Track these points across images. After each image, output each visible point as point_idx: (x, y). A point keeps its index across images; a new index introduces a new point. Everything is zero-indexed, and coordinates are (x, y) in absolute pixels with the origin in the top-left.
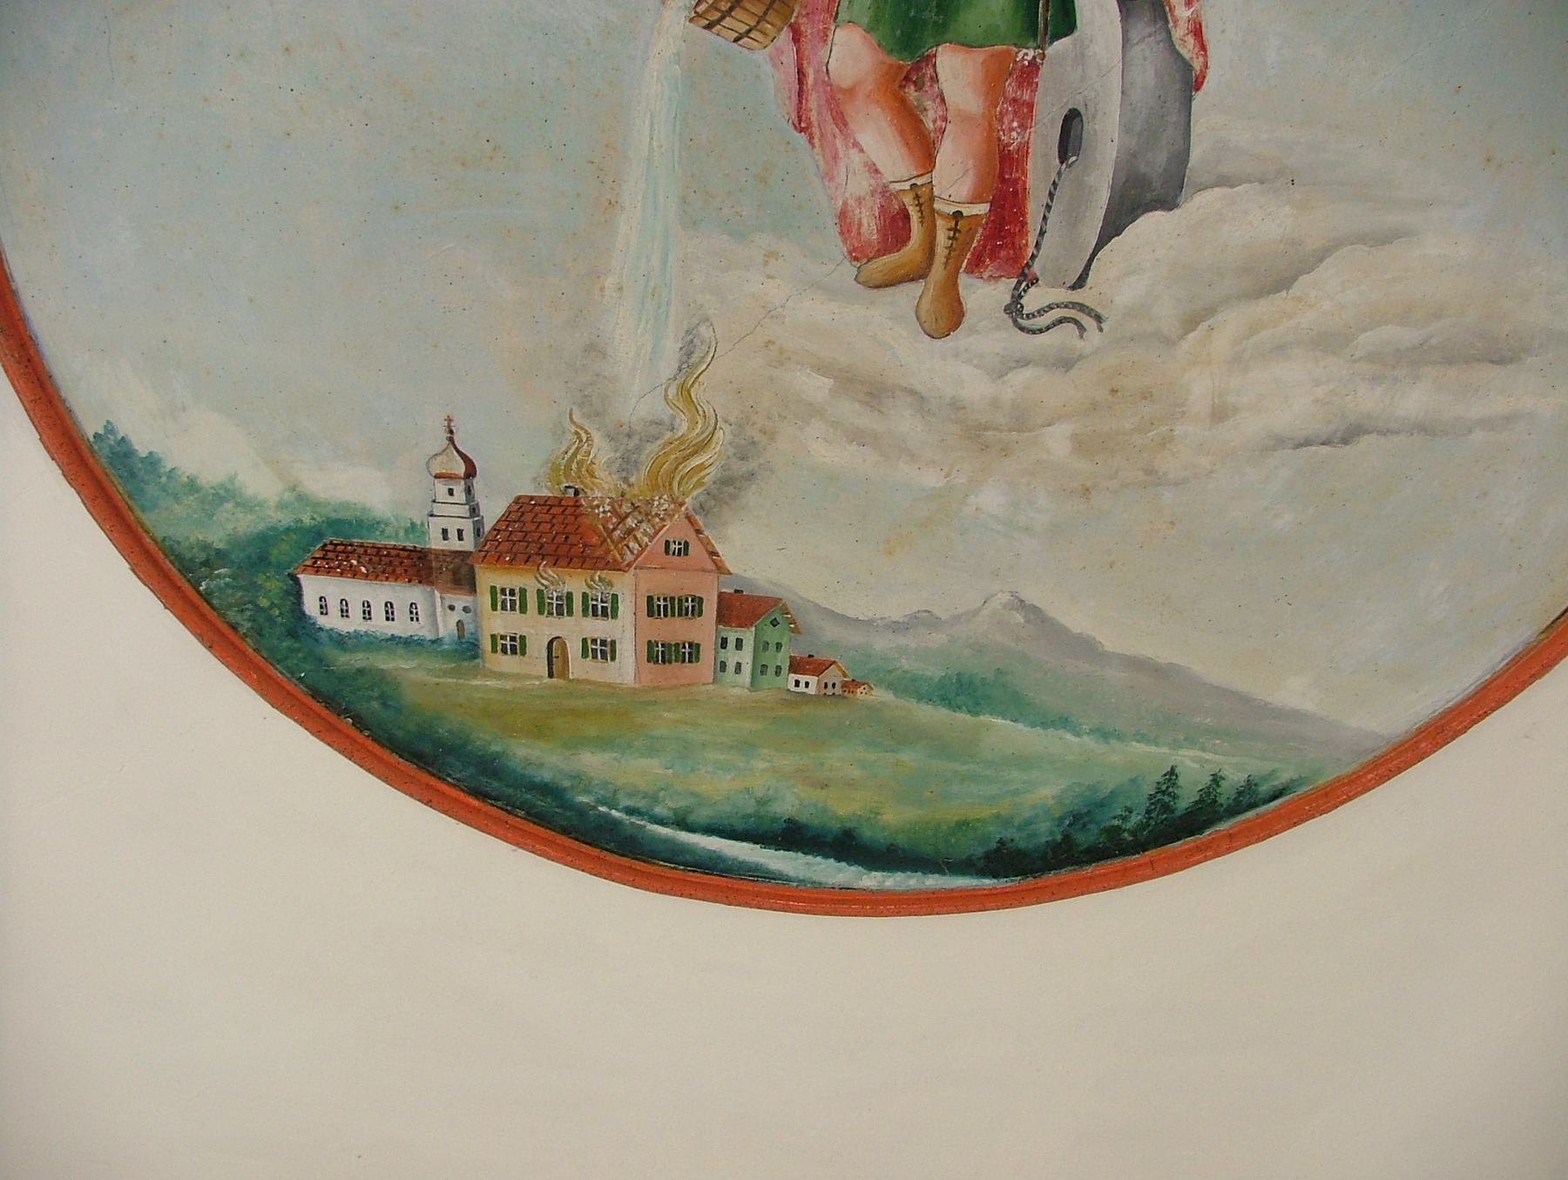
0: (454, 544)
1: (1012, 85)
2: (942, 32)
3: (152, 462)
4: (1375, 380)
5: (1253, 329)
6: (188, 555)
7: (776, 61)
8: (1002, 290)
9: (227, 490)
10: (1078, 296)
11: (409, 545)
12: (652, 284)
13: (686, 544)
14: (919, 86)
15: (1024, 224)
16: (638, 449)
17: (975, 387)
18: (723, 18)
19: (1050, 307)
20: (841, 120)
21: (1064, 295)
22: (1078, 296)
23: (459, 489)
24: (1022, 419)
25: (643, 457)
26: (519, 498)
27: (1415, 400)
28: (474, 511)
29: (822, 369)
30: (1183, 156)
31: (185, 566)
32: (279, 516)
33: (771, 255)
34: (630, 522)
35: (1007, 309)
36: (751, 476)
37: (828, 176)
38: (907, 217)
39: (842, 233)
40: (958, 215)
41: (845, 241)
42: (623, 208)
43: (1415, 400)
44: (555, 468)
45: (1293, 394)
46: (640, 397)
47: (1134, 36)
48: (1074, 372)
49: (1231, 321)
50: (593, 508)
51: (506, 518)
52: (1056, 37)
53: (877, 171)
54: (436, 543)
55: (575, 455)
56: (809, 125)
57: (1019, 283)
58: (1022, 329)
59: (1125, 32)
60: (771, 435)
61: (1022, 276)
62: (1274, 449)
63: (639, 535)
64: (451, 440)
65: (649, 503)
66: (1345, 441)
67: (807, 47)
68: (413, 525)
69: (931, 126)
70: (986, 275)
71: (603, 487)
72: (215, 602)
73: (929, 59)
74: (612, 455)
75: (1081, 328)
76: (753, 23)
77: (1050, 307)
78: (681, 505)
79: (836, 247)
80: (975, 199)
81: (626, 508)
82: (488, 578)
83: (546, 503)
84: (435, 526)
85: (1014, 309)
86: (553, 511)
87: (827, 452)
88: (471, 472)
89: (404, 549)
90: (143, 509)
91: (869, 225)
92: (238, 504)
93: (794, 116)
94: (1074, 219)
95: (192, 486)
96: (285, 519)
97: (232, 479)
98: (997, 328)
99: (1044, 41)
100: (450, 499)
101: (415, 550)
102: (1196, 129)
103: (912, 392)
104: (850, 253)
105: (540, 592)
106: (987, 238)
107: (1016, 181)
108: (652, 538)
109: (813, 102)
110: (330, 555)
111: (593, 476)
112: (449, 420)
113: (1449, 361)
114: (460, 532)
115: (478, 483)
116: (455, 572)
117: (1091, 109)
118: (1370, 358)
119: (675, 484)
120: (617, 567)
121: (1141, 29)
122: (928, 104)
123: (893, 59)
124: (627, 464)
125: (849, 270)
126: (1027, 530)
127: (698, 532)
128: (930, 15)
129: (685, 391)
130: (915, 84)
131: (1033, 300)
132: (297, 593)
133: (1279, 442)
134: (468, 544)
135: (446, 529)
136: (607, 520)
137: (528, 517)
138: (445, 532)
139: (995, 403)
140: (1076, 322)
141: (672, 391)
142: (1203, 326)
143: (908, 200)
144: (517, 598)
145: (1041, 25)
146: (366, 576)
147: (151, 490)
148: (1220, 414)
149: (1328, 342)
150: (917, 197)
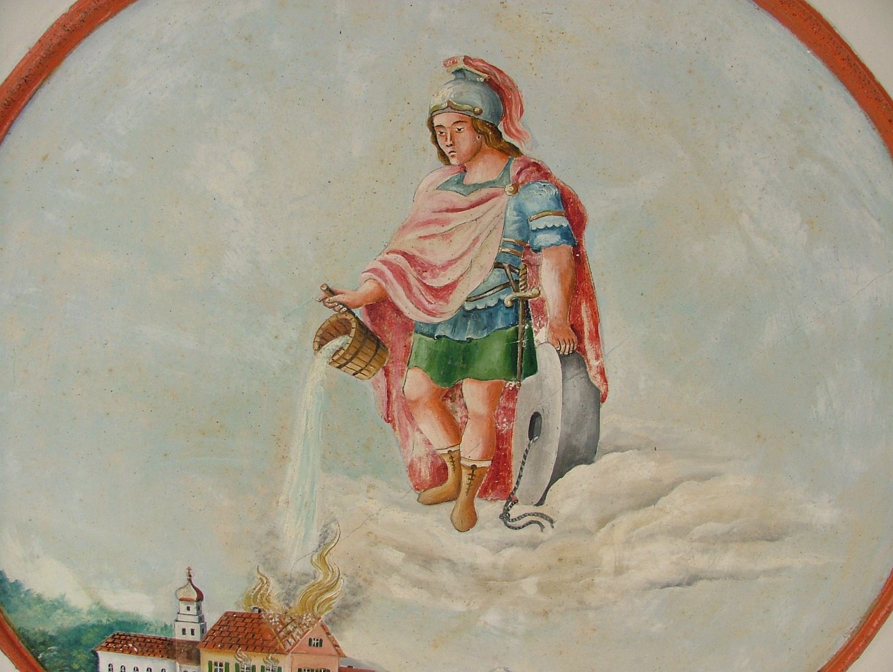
0: (189, 637)
1: (503, 400)
2: (465, 372)
3: (17, 585)
4: (704, 551)
5: (636, 526)
6: (33, 638)
7: (376, 386)
8: (498, 506)
9: (59, 603)
10: (539, 510)
11: (163, 637)
12: (305, 501)
13: (321, 641)
14: (453, 400)
15: (510, 472)
16: (295, 588)
17: (484, 558)
18: (347, 363)
19: (525, 515)
20: (410, 417)
21: (532, 509)
22: (539, 510)
23: (193, 607)
24: (510, 575)
25: (298, 593)
26: (227, 613)
27: (726, 561)
28: (201, 619)
29: (399, 547)
30: (596, 436)
31: (32, 645)
32: (89, 618)
33: (371, 487)
34: (290, 628)
35: (501, 517)
36: (358, 604)
37: (403, 446)
38: (446, 468)
39: (410, 476)
40: (474, 467)
41: (412, 480)
42: (290, 460)
43: (726, 561)
44: (248, 597)
45: (660, 559)
46: (297, 558)
47: (568, 375)
48: (538, 549)
49: (624, 522)
50: (269, 619)
51: (219, 624)
52: (526, 375)
53: (430, 444)
54: (178, 636)
55: (260, 590)
56: (393, 419)
57: (507, 503)
58: (509, 527)
59: (563, 373)
60: (370, 583)
61: (509, 499)
62: (650, 589)
63: (294, 635)
64: (190, 580)
65: (301, 618)
66: (689, 584)
67: (392, 379)
68: (166, 626)
69: (459, 421)
70: (489, 499)
71: (275, 608)
72: (47, 665)
73: (459, 386)
74: (280, 591)
75: (542, 527)
76: (363, 366)
77: (525, 515)
78: (319, 619)
79: (407, 483)
80: (484, 458)
81: (287, 620)
82: (207, 656)
83: (243, 617)
84: (178, 627)
85: (505, 516)
86: (247, 620)
87: (400, 591)
88: (200, 597)
89: (160, 639)
90: (9, 612)
91: (425, 472)
92: (65, 611)
93: (385, 414)
94: (537, 469)
95: (39, 600)
96: (92, 620)
97: (63, 596)
98: (496, 526)
99: (520, 377)
100: (188, 613)
101: (166, 640)
102: (603, 422)
103: (449, 560)
104: (415, 486)
105: (237, 666)
106: (489, 480)
107: (506, 449)
108: (301, 637)
109: (395, 407)
110: (117, 641)
111: (269, 602)
112: (189, 569)
113: (744, 541)
114: (192, 631)
115: (204, 604)
116: (189, 653)
117: (546, 412)
118: (702, 539)
119: (316, 608)
120: (281, 652)
121: (572, 371)
122: (458, 409)
123: (439, 386)
124: (289, 596)
125: (414, 495)
126: (513, 634)
127: (328, 634)
128: (459, 364)
129: (322, 558)
130: (451, 398)
131: (515, 512)
132: (95, 662)
133: (652, 585)
134: (197, 637)
135: (187, 628)
136: (276, 626)
137: (232, 624)
138: (184, 630)
139: (494, 566)
140: (539, 523)
141: (315, 557)
142: (609, 525)
143: (446, 459)
144: (223, 668)
145: (519, 369)
146: (137, 653)
147: (15, 601)
148: (619, 571)
149: (678, 532)
150: (452, 457)
